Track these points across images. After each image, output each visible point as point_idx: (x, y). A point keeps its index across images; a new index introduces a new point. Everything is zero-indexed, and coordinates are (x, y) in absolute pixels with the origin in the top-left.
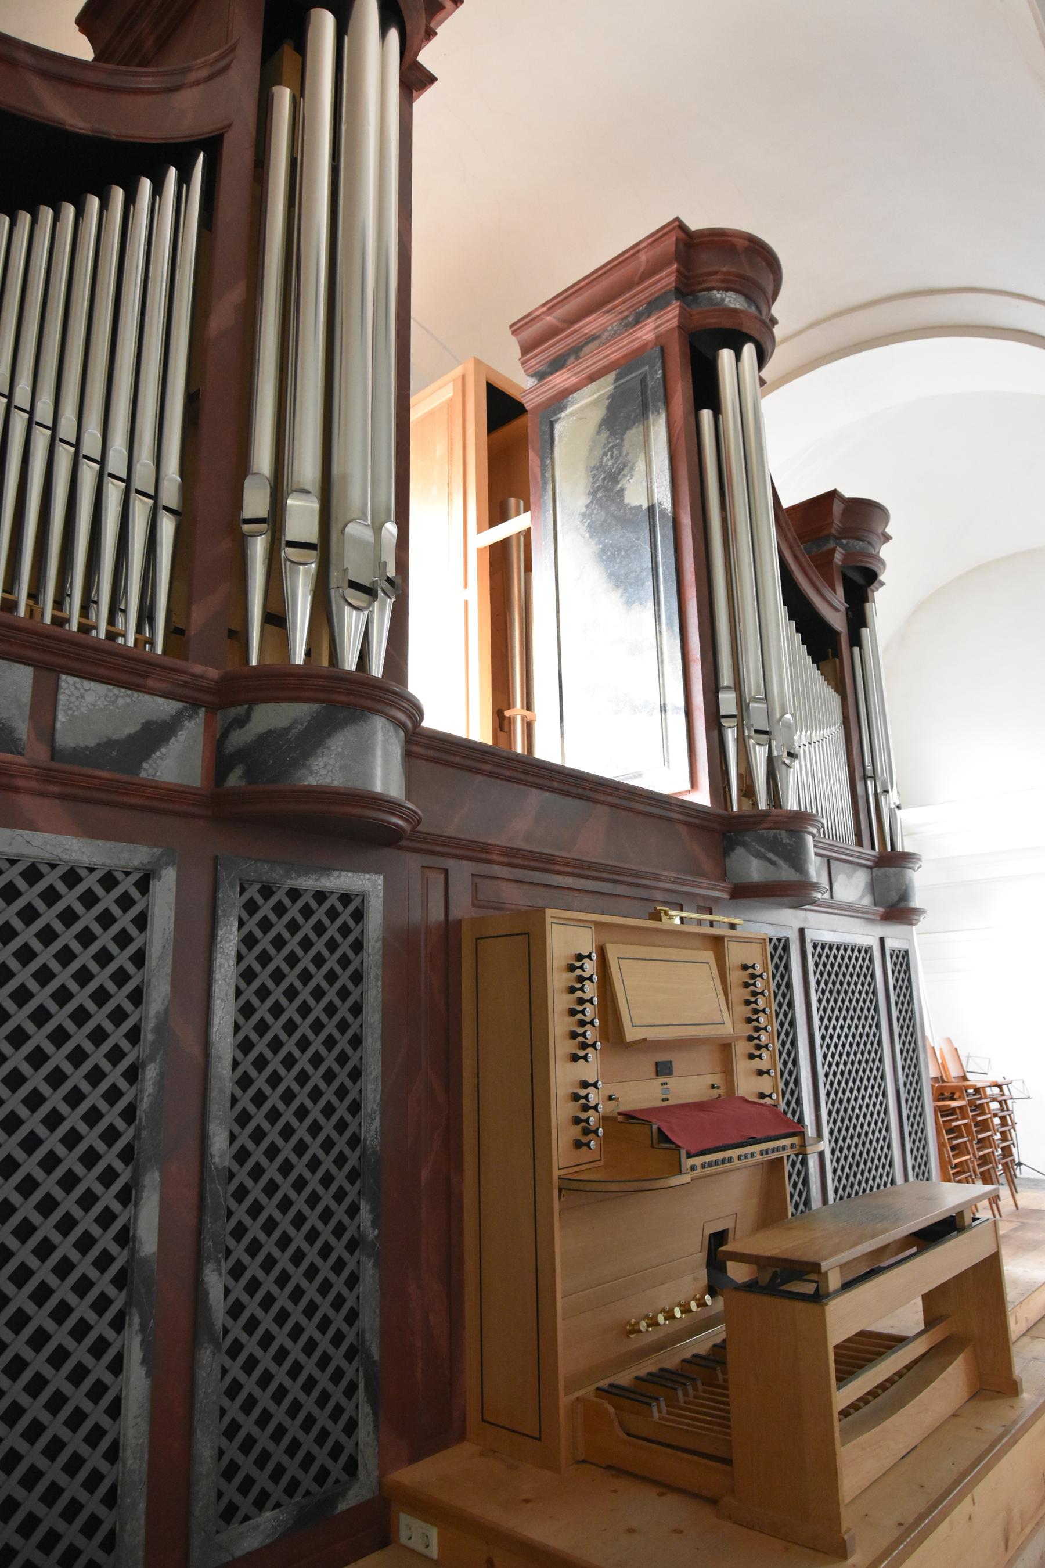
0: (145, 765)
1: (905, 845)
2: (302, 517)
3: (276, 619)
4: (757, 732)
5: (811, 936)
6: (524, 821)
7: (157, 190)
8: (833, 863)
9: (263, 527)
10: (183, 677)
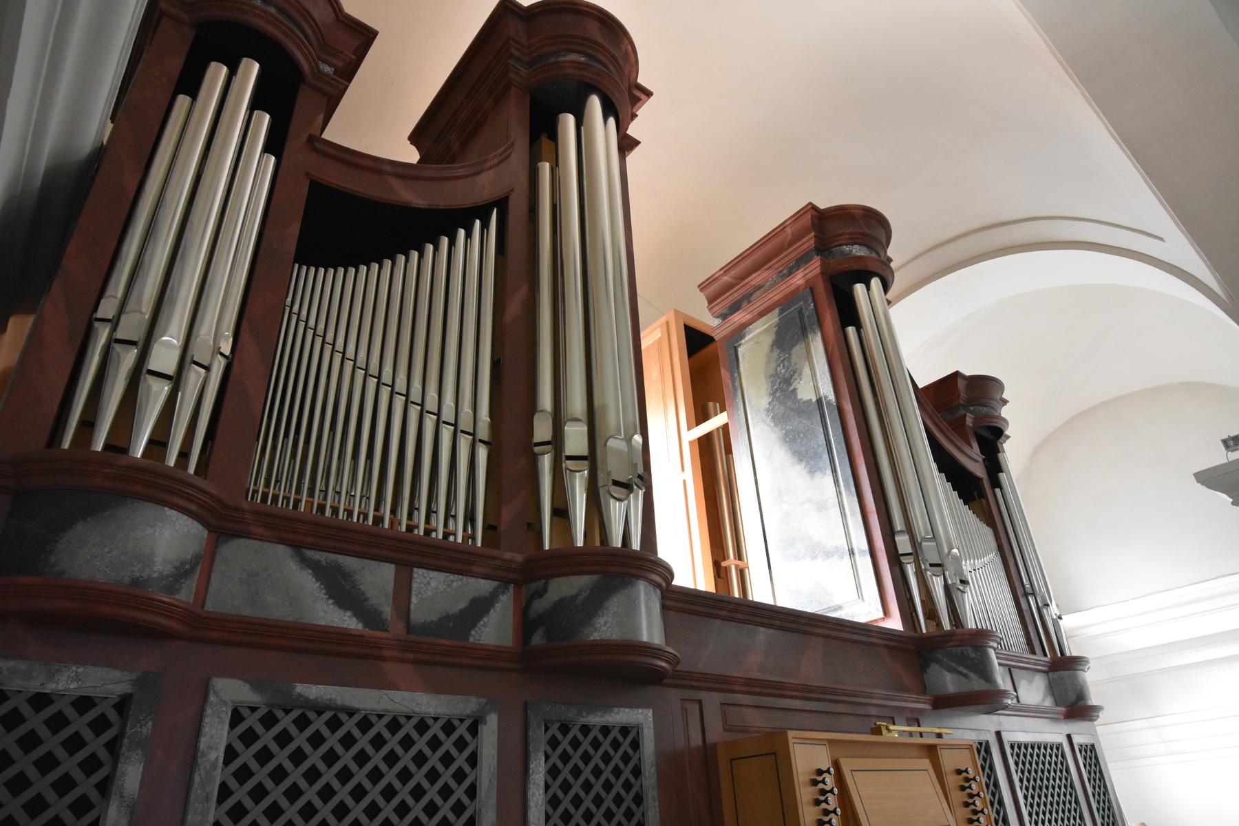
0: (473, 632)
1: (1072, 650)
2: (576, 439)
3: (562, 512)
4: (931, 565)
5: (1007, 737)
6: (756, 653)
7: (469, 235)
8: (1014, 671)
9: (549, 447)
10: (498, 563)
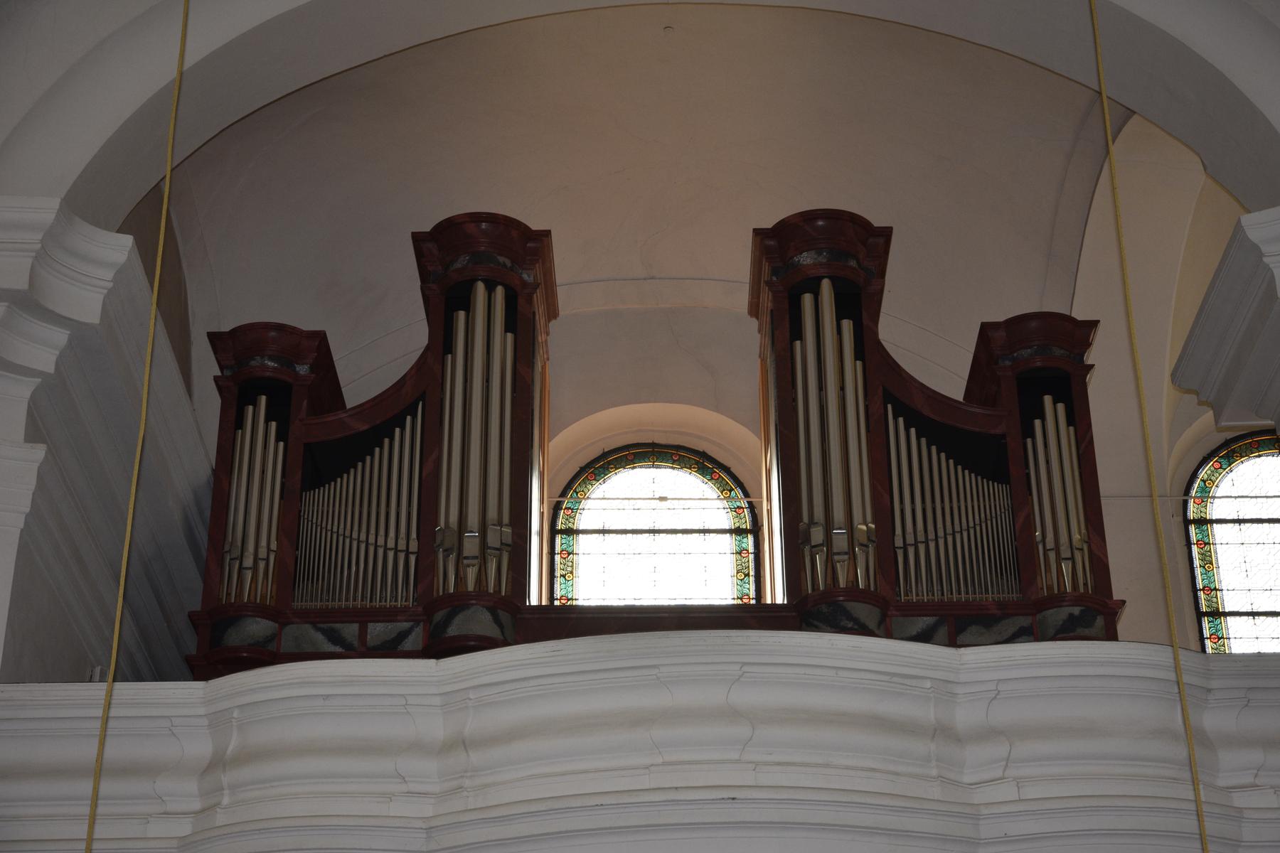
9: (475, 561)
